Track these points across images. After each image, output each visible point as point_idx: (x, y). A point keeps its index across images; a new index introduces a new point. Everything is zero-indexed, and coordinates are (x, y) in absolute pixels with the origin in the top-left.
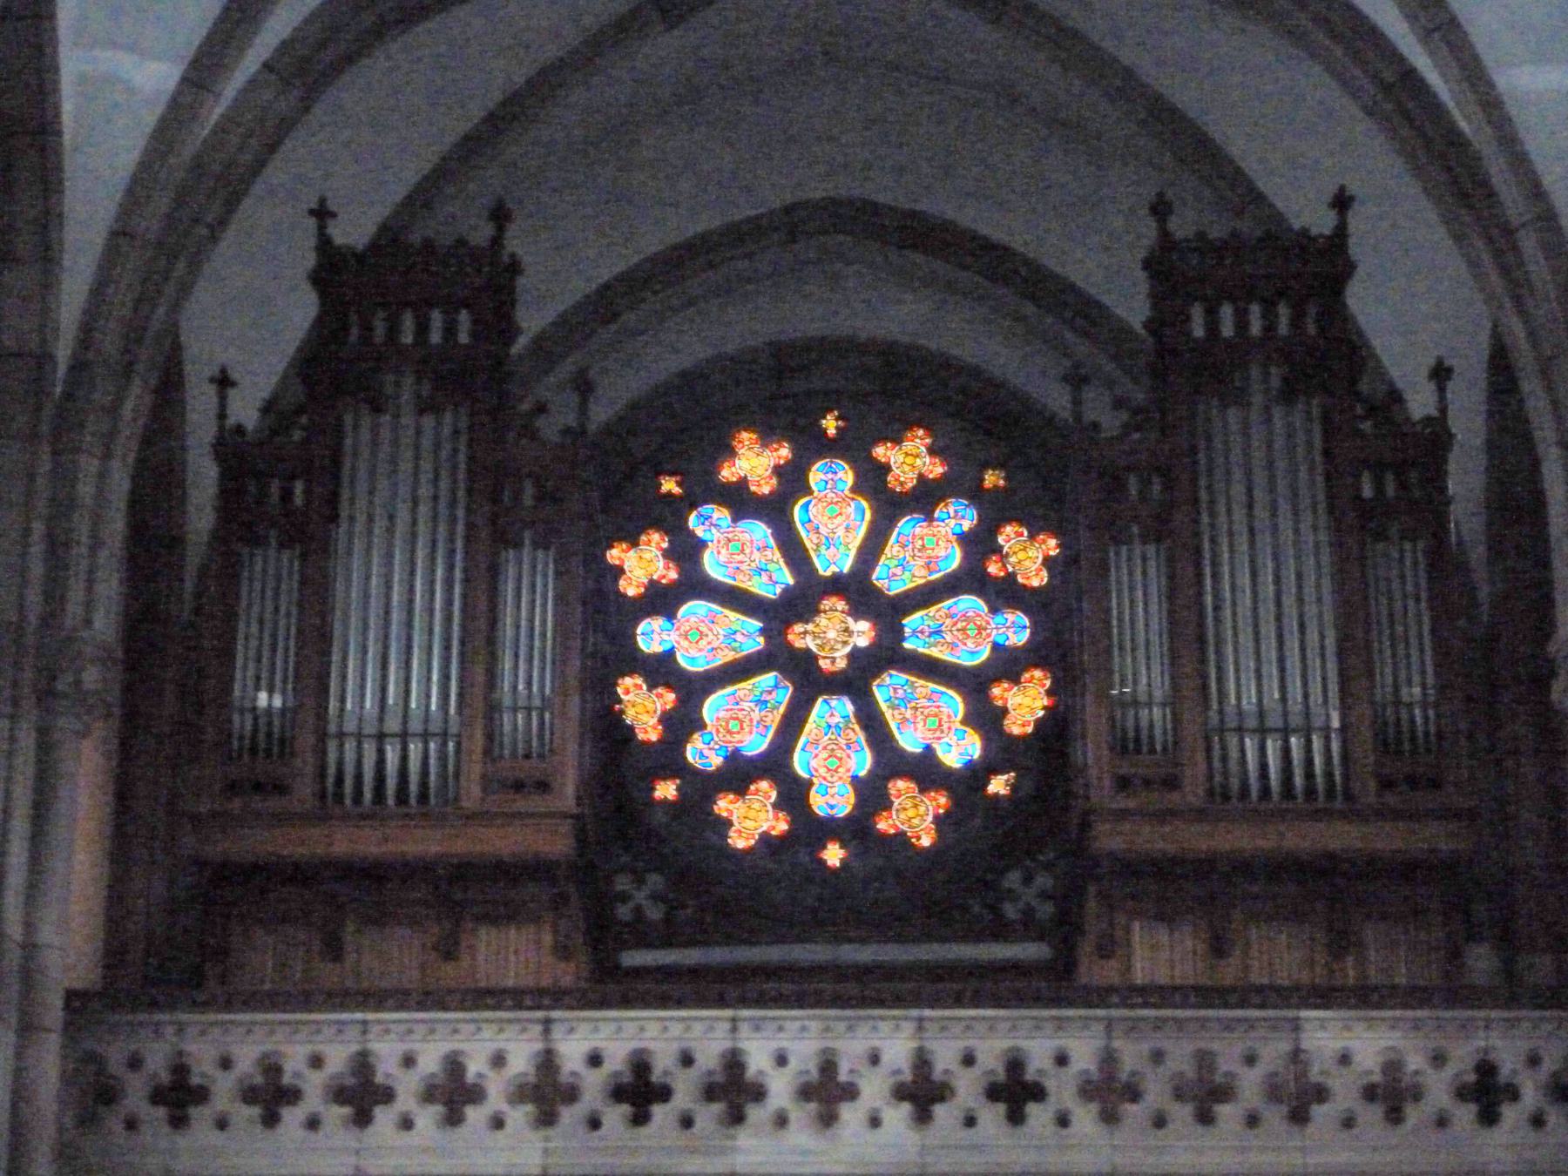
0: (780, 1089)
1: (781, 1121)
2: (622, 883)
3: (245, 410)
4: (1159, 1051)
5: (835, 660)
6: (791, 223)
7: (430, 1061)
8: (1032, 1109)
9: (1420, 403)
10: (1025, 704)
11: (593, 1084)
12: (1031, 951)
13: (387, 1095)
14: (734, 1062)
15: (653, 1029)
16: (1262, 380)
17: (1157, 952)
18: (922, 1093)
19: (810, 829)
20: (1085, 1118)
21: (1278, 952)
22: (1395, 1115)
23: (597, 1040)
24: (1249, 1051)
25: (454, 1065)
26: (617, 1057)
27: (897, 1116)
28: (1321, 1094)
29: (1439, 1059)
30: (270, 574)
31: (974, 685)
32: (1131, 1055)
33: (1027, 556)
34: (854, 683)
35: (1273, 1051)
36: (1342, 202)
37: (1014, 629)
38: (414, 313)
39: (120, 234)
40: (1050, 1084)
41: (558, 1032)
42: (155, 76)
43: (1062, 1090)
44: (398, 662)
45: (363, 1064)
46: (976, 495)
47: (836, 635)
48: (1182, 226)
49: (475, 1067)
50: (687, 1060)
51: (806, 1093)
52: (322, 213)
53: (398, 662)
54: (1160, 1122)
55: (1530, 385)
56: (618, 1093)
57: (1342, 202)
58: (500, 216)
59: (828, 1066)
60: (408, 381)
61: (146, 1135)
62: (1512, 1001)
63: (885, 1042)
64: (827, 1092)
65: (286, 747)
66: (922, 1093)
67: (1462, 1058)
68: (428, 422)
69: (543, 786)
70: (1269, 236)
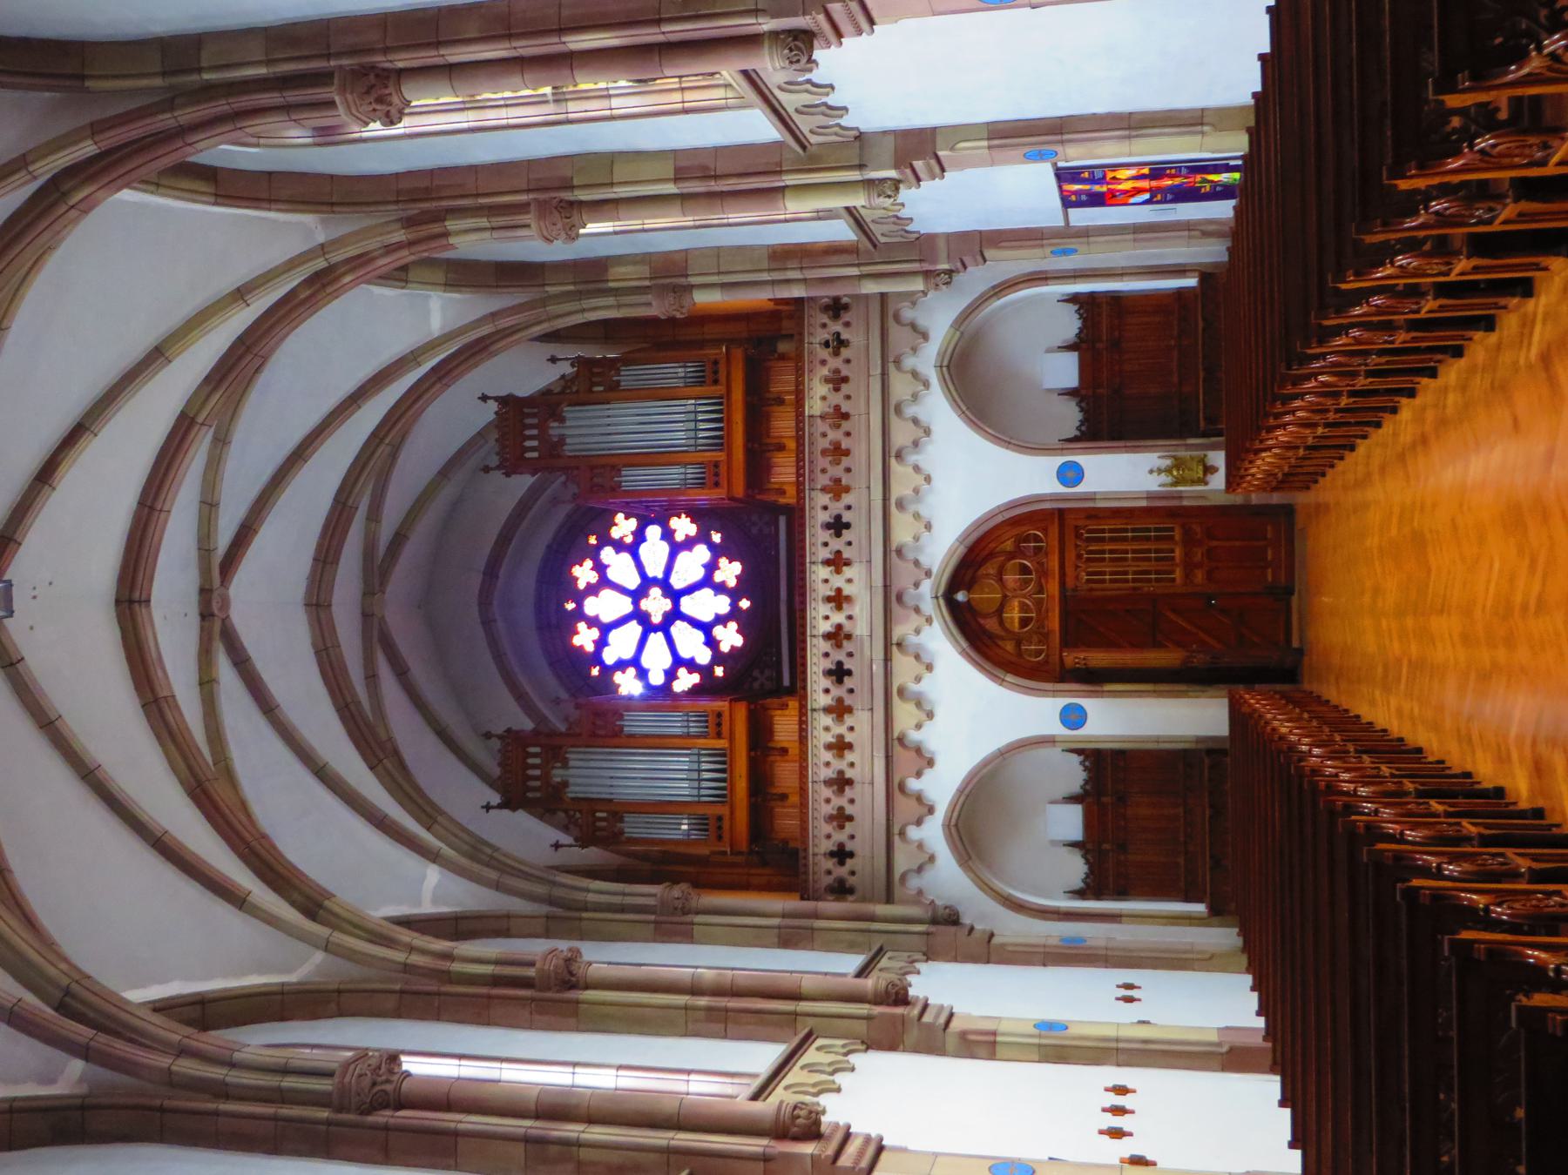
0: (838, 618)
1: (850, 617)
2: (756, 685)
3: (566, 839)
4: (823, 471)
5: (667, 605)
6: (487, 623)
7: (827, 756)
8: (844, 520)
9: (567, 369)
10: (683, 527)
11: (837, 692)
12: (782, 521)
13: (841, 809)
14: (828, 636)
15: (815, 669)
16: (555, 429)
17: (783, 472)
18: (837, 562)
19: (734, 614)
20: (847, 499)
21: (783, 425)
22: (845, 380)
23: (819, 691)
24: (822, 436)
25: (829, 747)
26: (826, 682)
27: (848, 572)
28: (837, 408)
29: (823, 362)
30: (635, 827)
31: (676, 549)
32: (823, 480)
33: (624, 527)
34: (675, 595)
35: (821, 426)
36: (484, 398)
37: (653, 532)
38: (526, 775)
39: (498, 886)
40: (835, 512)
41: (816, 706)
42: (433, 875)
43: (837, 507)
44: (668, 778)
45: (828, 783)
46: (599, 548)
47: (656, 604)
48: (494, 461)
49: (829, 738)
50: (826, 655)
51: (839, 608)
52: (488, 807)
53: (668, 778)
54: (848, 470)
55: (561, 324)
56: (840, 681)
57: (484, 398)
58: (488, 736)
59: (829, 599)
60: (555, 772)
61: (857, 869)
62: (801, 334)
63: (820, 577)
64: (838, 600)
65: (704, 818)
66: (837, 562)
67: (824, 353)
68: (571, 763)
69: (719, 715)
70: (497, 427)
